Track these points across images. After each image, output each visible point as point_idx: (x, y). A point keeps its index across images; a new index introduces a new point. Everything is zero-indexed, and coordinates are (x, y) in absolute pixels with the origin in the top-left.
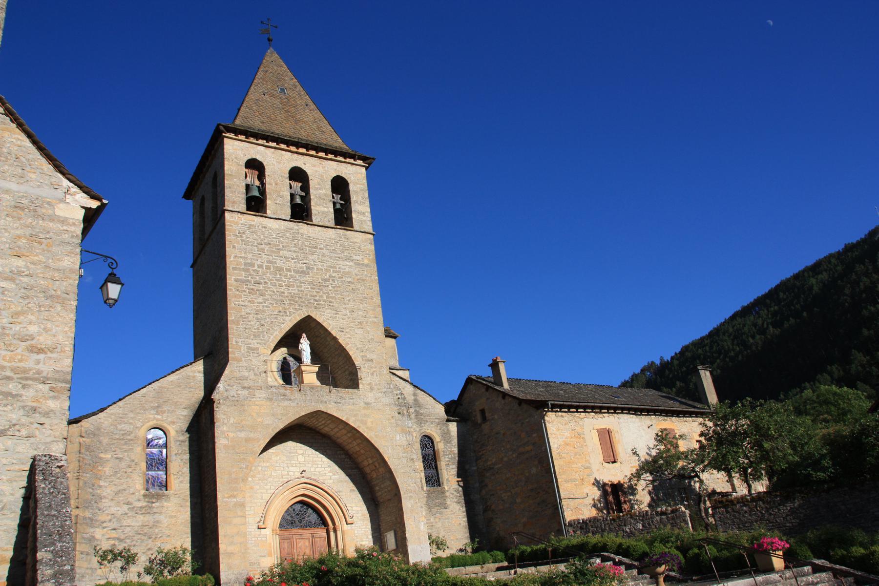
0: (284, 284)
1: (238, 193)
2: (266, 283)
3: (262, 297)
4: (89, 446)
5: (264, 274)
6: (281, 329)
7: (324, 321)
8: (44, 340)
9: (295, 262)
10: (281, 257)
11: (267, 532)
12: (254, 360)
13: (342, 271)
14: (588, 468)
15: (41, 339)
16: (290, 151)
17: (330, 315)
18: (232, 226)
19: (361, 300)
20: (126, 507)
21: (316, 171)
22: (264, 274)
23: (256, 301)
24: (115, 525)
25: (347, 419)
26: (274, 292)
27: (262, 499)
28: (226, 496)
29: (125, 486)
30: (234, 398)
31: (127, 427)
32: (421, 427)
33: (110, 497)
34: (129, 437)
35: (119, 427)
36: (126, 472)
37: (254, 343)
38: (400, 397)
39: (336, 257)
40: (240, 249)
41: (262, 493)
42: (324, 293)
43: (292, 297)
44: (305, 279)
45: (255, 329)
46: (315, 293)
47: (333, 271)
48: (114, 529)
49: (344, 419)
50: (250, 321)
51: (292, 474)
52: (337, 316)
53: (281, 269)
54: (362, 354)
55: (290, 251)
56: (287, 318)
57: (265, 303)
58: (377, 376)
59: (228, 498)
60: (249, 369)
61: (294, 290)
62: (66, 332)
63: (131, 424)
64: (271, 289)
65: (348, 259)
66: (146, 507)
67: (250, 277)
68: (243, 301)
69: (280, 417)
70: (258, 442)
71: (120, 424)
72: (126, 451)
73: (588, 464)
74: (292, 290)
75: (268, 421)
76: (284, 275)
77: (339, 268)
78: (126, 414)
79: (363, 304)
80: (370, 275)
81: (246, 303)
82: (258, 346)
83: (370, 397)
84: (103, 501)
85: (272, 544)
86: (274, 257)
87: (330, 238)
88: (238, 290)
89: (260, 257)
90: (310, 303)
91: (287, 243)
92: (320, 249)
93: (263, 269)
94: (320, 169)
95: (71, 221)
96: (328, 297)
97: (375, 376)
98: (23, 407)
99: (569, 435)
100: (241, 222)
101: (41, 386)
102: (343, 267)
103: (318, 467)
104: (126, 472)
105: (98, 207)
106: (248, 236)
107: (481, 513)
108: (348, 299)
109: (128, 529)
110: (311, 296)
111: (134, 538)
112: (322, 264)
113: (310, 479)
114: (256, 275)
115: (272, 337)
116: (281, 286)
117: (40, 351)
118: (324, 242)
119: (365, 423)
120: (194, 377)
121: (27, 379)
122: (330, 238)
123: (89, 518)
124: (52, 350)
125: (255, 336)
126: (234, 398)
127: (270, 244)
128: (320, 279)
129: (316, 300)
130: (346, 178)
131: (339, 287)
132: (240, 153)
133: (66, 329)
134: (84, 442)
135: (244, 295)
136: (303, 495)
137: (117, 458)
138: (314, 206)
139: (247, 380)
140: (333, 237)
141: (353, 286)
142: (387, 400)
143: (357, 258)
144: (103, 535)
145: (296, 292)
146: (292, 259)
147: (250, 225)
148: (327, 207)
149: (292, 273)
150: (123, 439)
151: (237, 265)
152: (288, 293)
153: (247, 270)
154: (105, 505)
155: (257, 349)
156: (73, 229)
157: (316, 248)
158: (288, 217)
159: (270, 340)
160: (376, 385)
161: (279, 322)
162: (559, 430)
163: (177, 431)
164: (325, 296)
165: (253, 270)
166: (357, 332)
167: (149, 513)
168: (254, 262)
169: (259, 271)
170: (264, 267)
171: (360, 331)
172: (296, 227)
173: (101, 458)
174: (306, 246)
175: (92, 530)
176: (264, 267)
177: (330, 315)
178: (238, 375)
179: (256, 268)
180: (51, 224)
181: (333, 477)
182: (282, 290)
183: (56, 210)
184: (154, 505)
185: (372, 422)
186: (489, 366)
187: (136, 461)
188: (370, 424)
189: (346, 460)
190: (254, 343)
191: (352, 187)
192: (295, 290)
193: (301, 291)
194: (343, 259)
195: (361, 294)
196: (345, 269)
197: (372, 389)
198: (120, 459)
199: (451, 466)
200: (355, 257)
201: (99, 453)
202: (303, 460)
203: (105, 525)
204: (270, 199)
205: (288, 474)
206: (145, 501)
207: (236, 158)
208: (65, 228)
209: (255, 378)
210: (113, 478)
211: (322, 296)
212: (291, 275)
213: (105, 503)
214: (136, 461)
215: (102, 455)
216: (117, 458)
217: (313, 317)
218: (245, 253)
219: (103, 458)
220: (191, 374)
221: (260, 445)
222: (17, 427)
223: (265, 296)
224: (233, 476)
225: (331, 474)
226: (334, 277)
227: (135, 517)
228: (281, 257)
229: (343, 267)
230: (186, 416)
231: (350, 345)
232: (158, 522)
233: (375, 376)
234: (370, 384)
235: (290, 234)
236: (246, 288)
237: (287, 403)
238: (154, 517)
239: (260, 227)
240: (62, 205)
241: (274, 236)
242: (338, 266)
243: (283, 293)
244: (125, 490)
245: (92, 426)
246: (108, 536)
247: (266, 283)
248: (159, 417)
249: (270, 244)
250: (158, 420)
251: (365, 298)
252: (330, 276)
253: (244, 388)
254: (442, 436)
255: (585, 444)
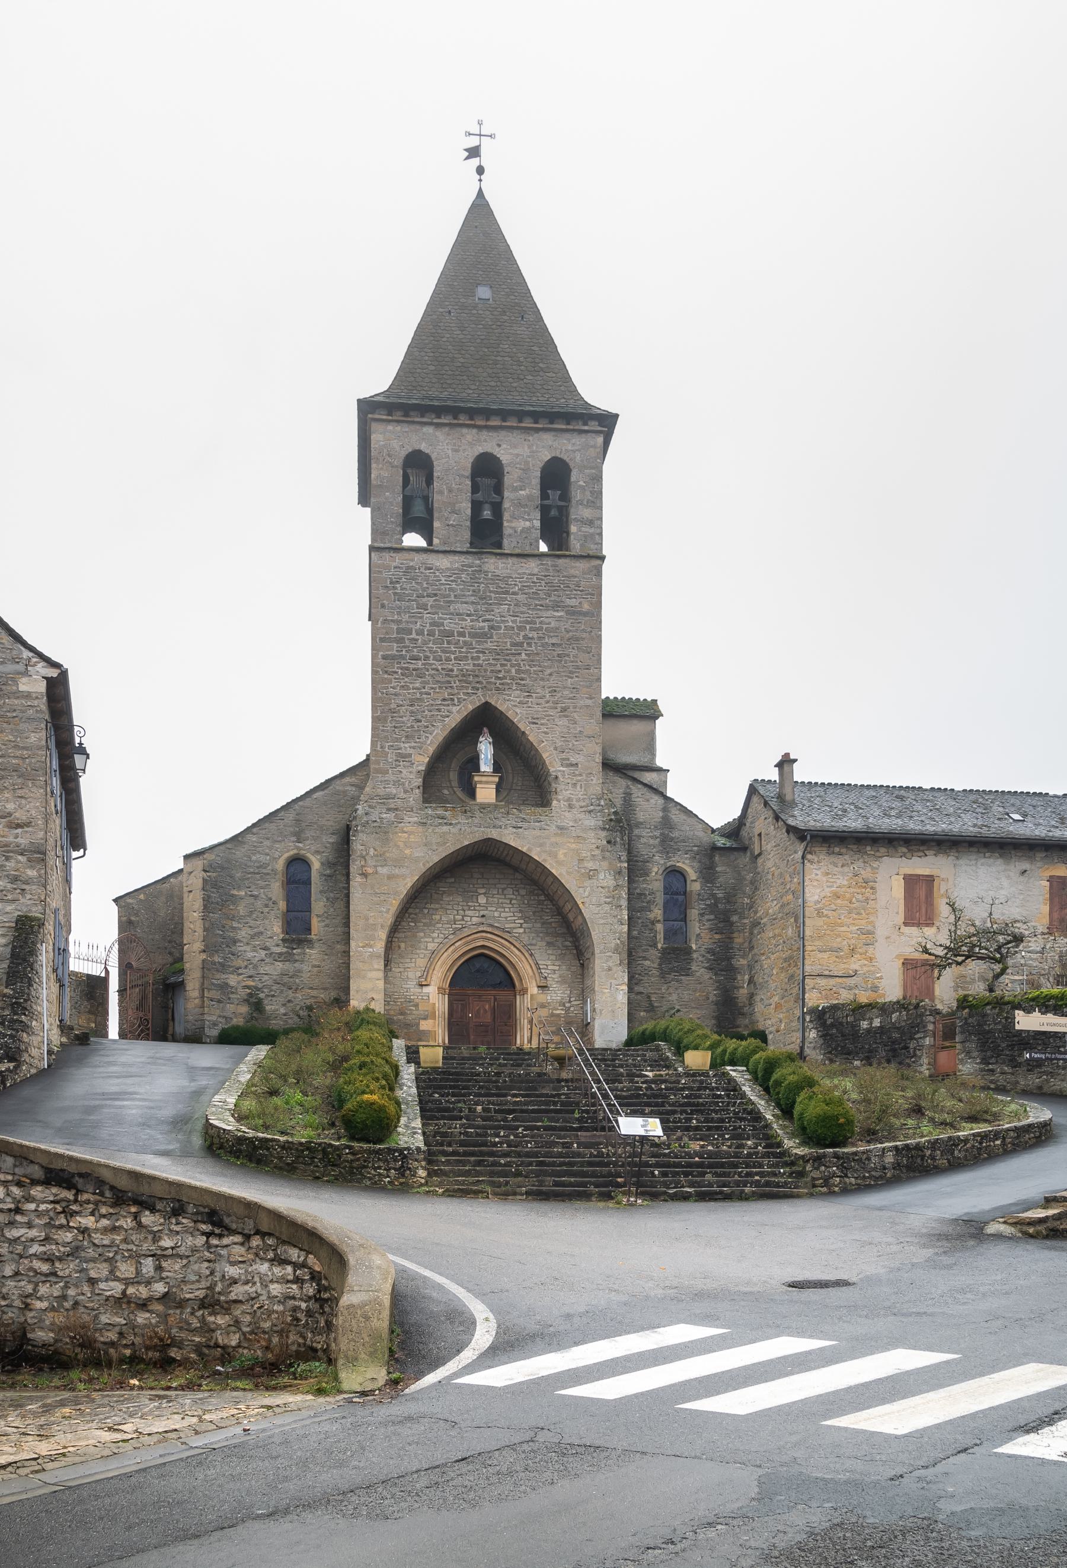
0: (453, 657)
1: (391, 517)
2: (427, 658)
3: (420, 680)
4: (216, 881)
5: (425, 643)
6: (444, 726)
7: (508, 709)
8: (20, 816)
9: (472, 621)
10: (452, 614)
11: (432, 990)
12: (404, 771)
13: (545, 626)
14: (869, 933)
15: (17, 815)
16: (474, 426)
17: (518, 700)
18: (380, 572)
19: (571, 672)
20: (263, 953)
21: (518, 455)
22: (425, 643)
23: (411, 686)
24: (252, 972)
25: (530, 849)
26: (438, 670)
27: (426, 949)
28: (361, 945)
29: (261, 929)
30: (375, 824)
31: (263, 858)
32: (668, 858)
33: (245, 940)
34: (264, 871)
35: (254, 858)
36: (262, 913)
37: (406, 747)
38: (613, 817)
39: (536, 605)
40: (392, 608)
41: (427, 942)
42: (512, 666)
43: (463, 675)
44: (486, 646)
45: (408, 728)
46: (498, 667)
47: (530, 628)
48: (250, 977)
49: (524, 850)
50: (402, 717)
51: (469, 918)
52: (530, 700)
53: (450, 634)
54: (564, 756)
55: (466, 603)
56: (455, 708)
57: (424, 688)
58: (581, 788)
59: (363, 947)
60: (397, 783)
61: (468, 666)
62: (37, 807)
63: (267, 855)
64: (434, 666)
65: (556, 606)
66: (285, 953)
67: (404, 650)
68: (393, 688)
69: (435, 847)
70: (404, 879)
71: (254, 854)
72: (262, 888)
73: (870, 927)
74: (465, 665)
75: (418, 853)
76: (454, 642)
77: (541, 623)
78: (261, 843)
79: (572, 678)
80: (589, 629)
81: (398, 690)
82: (411, 751)
83: (567, 818)
84: (238, 944)
85: (437, 1005)
86: (441, 615)
87: (530, 575)
88: (386, 672)
89: (421, 618)
90: (490, 682)
91: (462, 590)
92: (514, 593)
93: (424, 635)
94: (524, 450)
95: (34, 695)
96: (518, 671)
97: (578, 787)
98: (7, 876)
99: (845, 883)
100: (394, 564)
101: (20, 857)
102: (547, 620)
103: (504, 912)
104: (262, 913)
105: (59, 674)
106: (404, 586)
107: (745, 986)
108: (548, 671)
109: (266, 977)
110: (492, 671)
111: (274, 988)
112: (513, 618)
113: (492, 926)
114: (414, 647)
115: (431, 738)
116: (448, 659)
117: (18, 826)
118: (520, 582)
119: (555, 856)
120: (345, 792)
121: (8, 852)
122: (530, 575)
123: (219, 962)
124: (28, 824)
125: (407, 737)
126: (375, 824)
127: (436, 595)
128: (509, 644)
129: (499, 678)
130: (567, 460)
131: (537, 654)
132: (395, 444)
133: (38, 804)
134: (209, 877)
135: (395, 679)
136: (483, 947)
137: (251, 896)
138: (508, 521)
139: (393, 798)
140: (536, 571)
141: (559, 651)
142: (590, 822)
143: (573, 602)
144: (239, 983)
145: (471, 667)
146: (468, 615)
147: (408, 568)
148: (530, 520)
149: (467, 639)
150: (258, 873)
151: (387, 633)
152: (458, 670)
153: (400, 641)
154: (240, 949)
155: (410, 755)
156: (36, 703)
157: (507, 593)
158: (466, 547)
159: (429, 742)
160: (578, 800)
161: (441, 716)
162: (828, 874)
163: (322, 864)
164: (513, 671)
165: (408, 639)
166: (558, 723)
167: (289, 961)
168: (411, 626)
169: (417, 640)
170: (426, 633)
171: (563, 722)
172: (478, 562)
173: (233, 896)
174: (491, 592)
175: (224, 976)
176: (426, 633)
177: (518, 700)
178: (381, 791)
179: (414, 636)
180: (16, 702)
181: (525, 925)
182: (451, 667)
183: (20, 685)
184: (295, 951)
185: (565, 855)
186: (775, 766)
187: (274, 899)
188: (562, 856)
189: (545, 903)
190: (406, 747)
191: (574, 476)
192: (469, 664)
193: (479, 665)
194: (547, 608)
195: (572, 662)
196: (549, 623)
197: (570, 806)
198: (256, 897)
199: (707, 917)
200: (568, 602)
201: (230, 889)
202: (485, 901)
203: (240, 971)
204: (439, 519)
205: (463, 920)
206: (284, 947)
207: (389, 455)
208: (29, 703)
209: (405, 796)
210: (249, 920)
211: (509, 671)
212: (465, 642)
213: (241, 947)
214: (274, 899)
215: (235, 892)
216: (251, 896)
217: (493, 703)
218: (399, 614)
219: (236, 895)
220: (341, 788)
221: (406, 884)
222: (4, 892)
223: (425, 677)
224: (371, 921)
225: (522, 921)
226: (532, 638)
227: (273, 964)
228: (452, 614)
229: (547, 620)
230: (333, 843)
231: (545, 743)
232: (300, 971)
233: (578, 787)
234: (569, 799)
235: (468, 574)
236: (398, 668)
237: (445, 828)
238: (295, 965)
239: (422, 570)
240: (24, 680)
241: (443, 582)
242: (538, 620)
243: (452, 670)
244: (262, 933)
245: (219, 858)
246: (244, 984)
247: (427, 658)
248: (300, 845)
249: (436, 595)
250: (298, 848)
251: (578, 667)
252: (526, 637)
253: (389, 810)
254: (701, 872)
255: (873, 897)
